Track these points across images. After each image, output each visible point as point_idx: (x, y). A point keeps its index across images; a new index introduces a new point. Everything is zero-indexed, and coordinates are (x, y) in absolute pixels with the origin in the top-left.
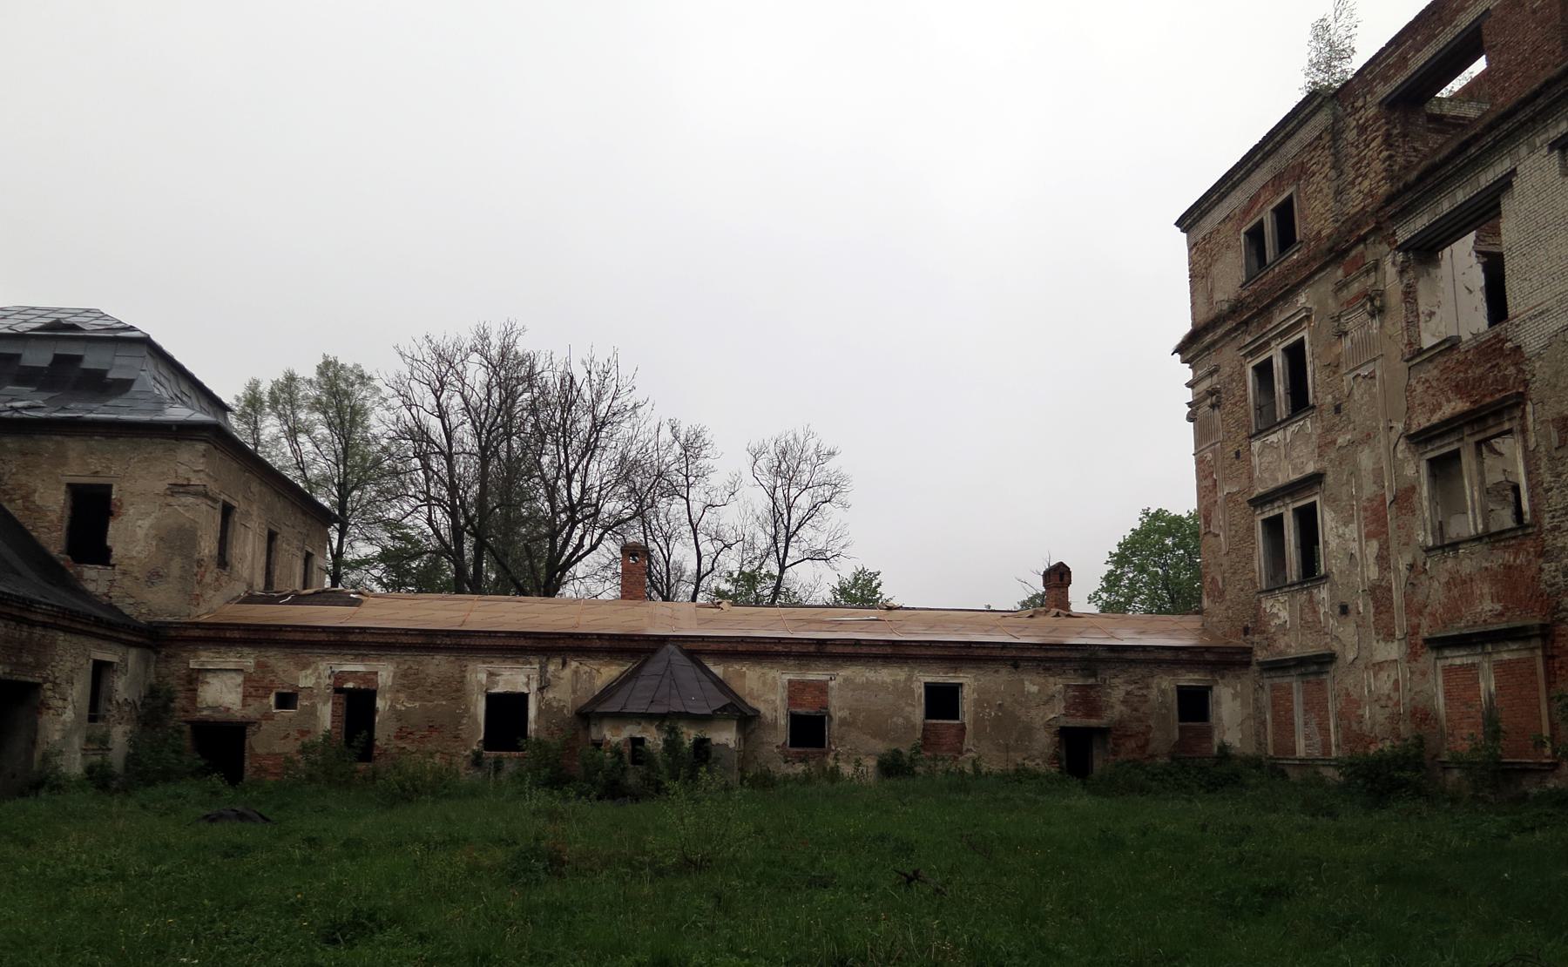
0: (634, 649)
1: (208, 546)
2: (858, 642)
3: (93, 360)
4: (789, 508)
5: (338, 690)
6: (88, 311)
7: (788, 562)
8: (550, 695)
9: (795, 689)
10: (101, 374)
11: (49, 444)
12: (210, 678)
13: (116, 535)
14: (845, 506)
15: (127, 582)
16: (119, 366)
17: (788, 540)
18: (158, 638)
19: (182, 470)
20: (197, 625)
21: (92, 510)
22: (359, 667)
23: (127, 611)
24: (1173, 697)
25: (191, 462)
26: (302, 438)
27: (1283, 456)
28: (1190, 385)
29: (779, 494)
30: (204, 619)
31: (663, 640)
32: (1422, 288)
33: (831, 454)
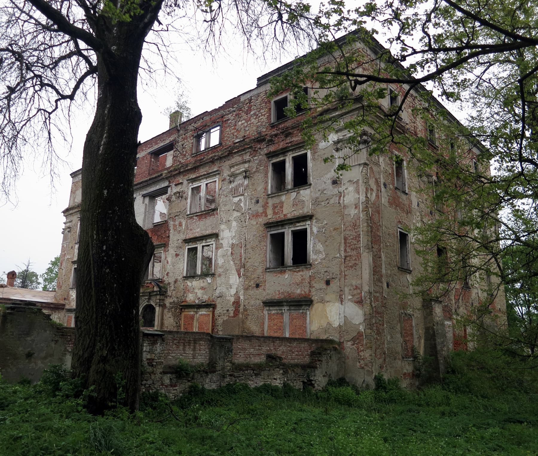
28: (65, 223)
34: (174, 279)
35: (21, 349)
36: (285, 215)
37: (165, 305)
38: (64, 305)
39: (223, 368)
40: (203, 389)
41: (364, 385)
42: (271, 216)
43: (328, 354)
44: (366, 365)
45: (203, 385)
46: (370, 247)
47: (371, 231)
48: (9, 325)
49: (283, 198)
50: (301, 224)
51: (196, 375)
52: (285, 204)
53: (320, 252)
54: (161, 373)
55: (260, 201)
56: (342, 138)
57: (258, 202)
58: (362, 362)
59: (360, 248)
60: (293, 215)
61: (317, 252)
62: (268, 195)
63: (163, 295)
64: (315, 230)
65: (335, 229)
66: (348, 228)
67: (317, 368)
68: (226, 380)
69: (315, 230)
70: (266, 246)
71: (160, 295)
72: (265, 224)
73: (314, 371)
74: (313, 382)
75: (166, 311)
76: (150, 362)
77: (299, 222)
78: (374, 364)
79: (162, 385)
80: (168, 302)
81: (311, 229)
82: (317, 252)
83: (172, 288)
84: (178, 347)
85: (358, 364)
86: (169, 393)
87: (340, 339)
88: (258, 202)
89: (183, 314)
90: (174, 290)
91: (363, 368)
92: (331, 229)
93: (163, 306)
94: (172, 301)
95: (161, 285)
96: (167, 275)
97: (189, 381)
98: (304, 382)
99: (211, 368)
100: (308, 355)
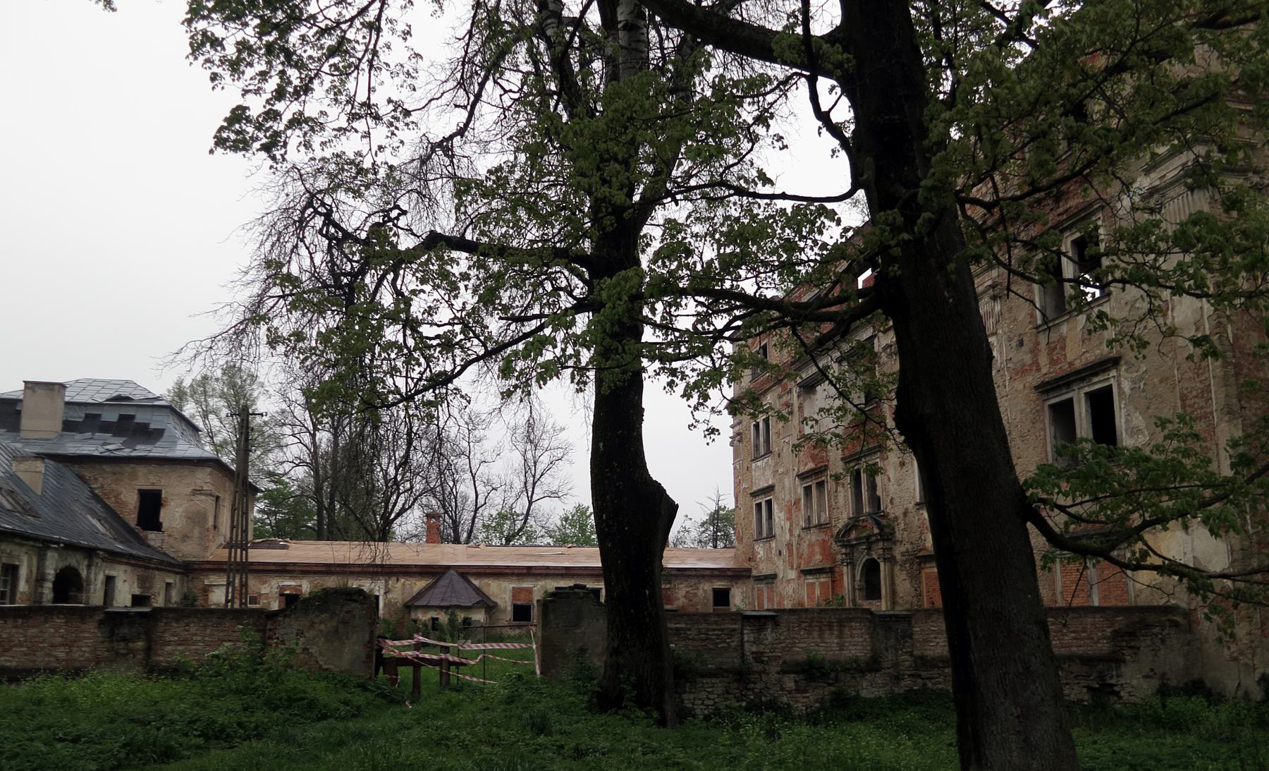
0: (434, 572)
1: (211, 522)
2: (548, 568)
3: (141, 418)
4: (535, 463)
5: (281, 595)
6: (127, 382)
7: (535, 497)
8: (390, 596)
9: (516, 592)
10: (146, 425)
11: (128, 468)
12: (215, 589)
13: (164, 516)
14: (571, 463)
15: (171, 541)
16: (156, 422)
17: (534, 484)
18: (189, 569)
19: (198, 482)
20: (209, 562)
21: (151, 504)
22: (293, 583)
23: (172, 555)
24: (710, 595)
25: (203, 478)
26: (211, 416)
27: (762, 475)
28: (732, 427)
29: (529, 455)
30: (210, 558)
31: (448, 567)
32: (806, 404)
33: (562, 429)
34: (902, 510)
35: (570, 644)
36: (1070, 364)
37: (893, 558)
38: (750, 570)
39: (896, 665)
40: (857, 697)
41: (1240, 693)
42: (1047, 370)
43: (1156, 635)
44: (1242, 654)
45: (858, 692)
46: (1237, 408)
47: (1237, 375)
48: (552, 616)
49: (1064, 329)
50: (1101, 378)
51: (842, 676)
52: (1068, 341)
53: (1139, 431)
54: (778, 673)
55: (1026, 340)
56: (1158, 183)
57: (1021, 343)
58: (1234, 647)
59: (1212, 413)
60: (1084, 361)
61: (1134, 432)
62: (1037, 327)
63: (888, 540)
64: (1126, 386)
65: (1162, 381)
66: (1186, 376)
67: (1124, 662)
68: (903, 683)
69: (1126, 386)
70: (1044, 430)
71: (883, 540)
72: (1036, 388)
73: (1118, 668)
74: (1116, 689)
75: (897, 568)
76: (758, 657)
77: (1096, 374)
78: (1259, 650)
79: (783, 689)
80: (898, 551)
81: (1119, 385)
82: (1134, 432)
83: (902, 526)
84: (810, 633)
85: (1226, 652)
86: (797, 702)
87: (1189, 604)
88: (1021, 343)
89: (924, 572)
90: (905, 530)
91: (1235, 659)
92: (1156, 380)
93: (891, 560)
94: (903, 549)
95: (884, 522)
96: (891, 502)
97: (830, 685)
98: (1090, 688)
99: (873, 665)
100: (1107, 638)
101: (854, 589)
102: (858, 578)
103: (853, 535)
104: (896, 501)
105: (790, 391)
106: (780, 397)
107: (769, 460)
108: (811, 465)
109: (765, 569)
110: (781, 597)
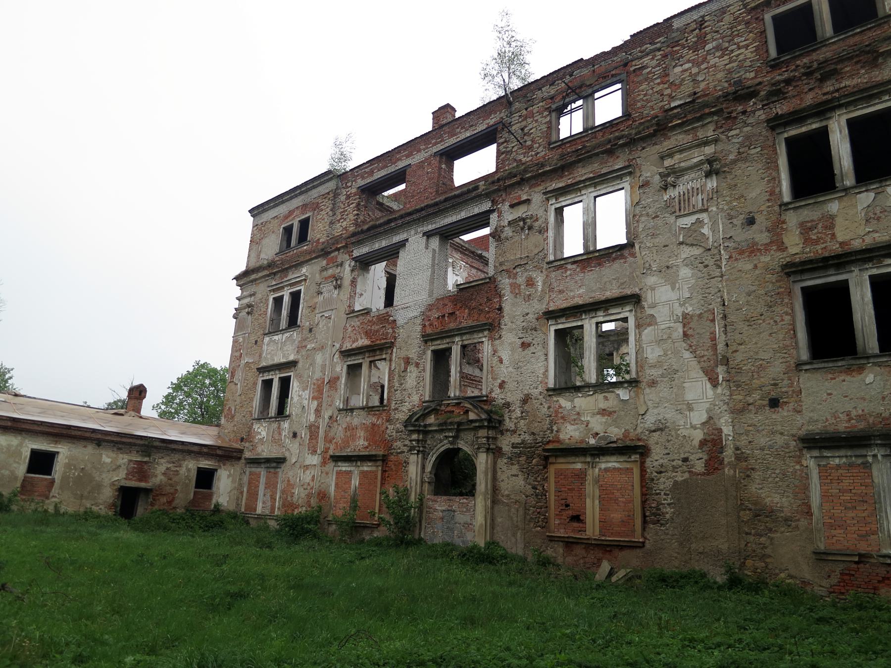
24: (194, 475)
27: (279, 348)
32: (359, 280)
38: (241, 451)
63: (494, 428)
80: (506, 443)
83: (518, 413)
94: (516, 440)
101: (422, 482)
102: (429, 468)
103: (431, 420)
104: (511, 385)
105: (341, 264)
106: (324, 269)
107: (295, 334)
108: (363, 342)
109: (265, 451)
110: (290, 485)
